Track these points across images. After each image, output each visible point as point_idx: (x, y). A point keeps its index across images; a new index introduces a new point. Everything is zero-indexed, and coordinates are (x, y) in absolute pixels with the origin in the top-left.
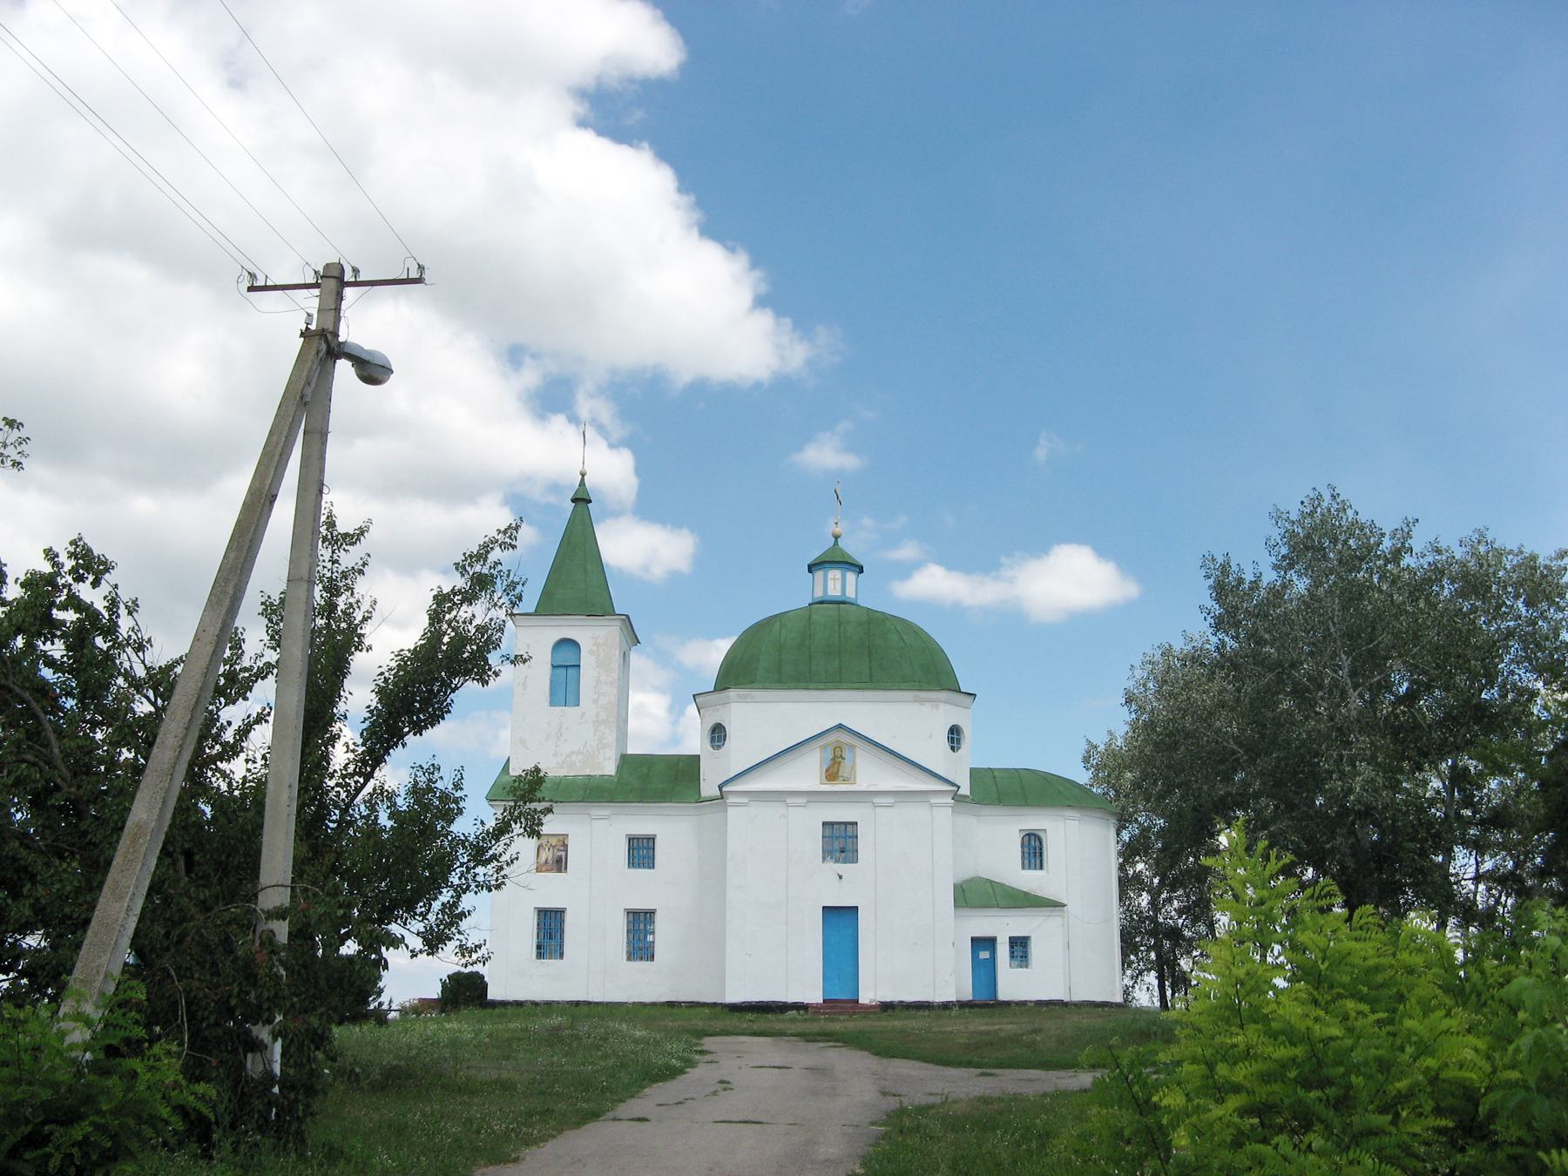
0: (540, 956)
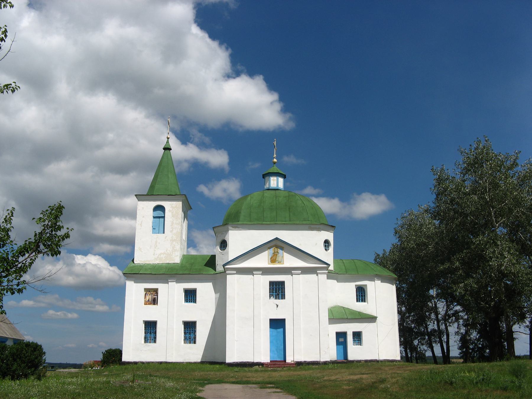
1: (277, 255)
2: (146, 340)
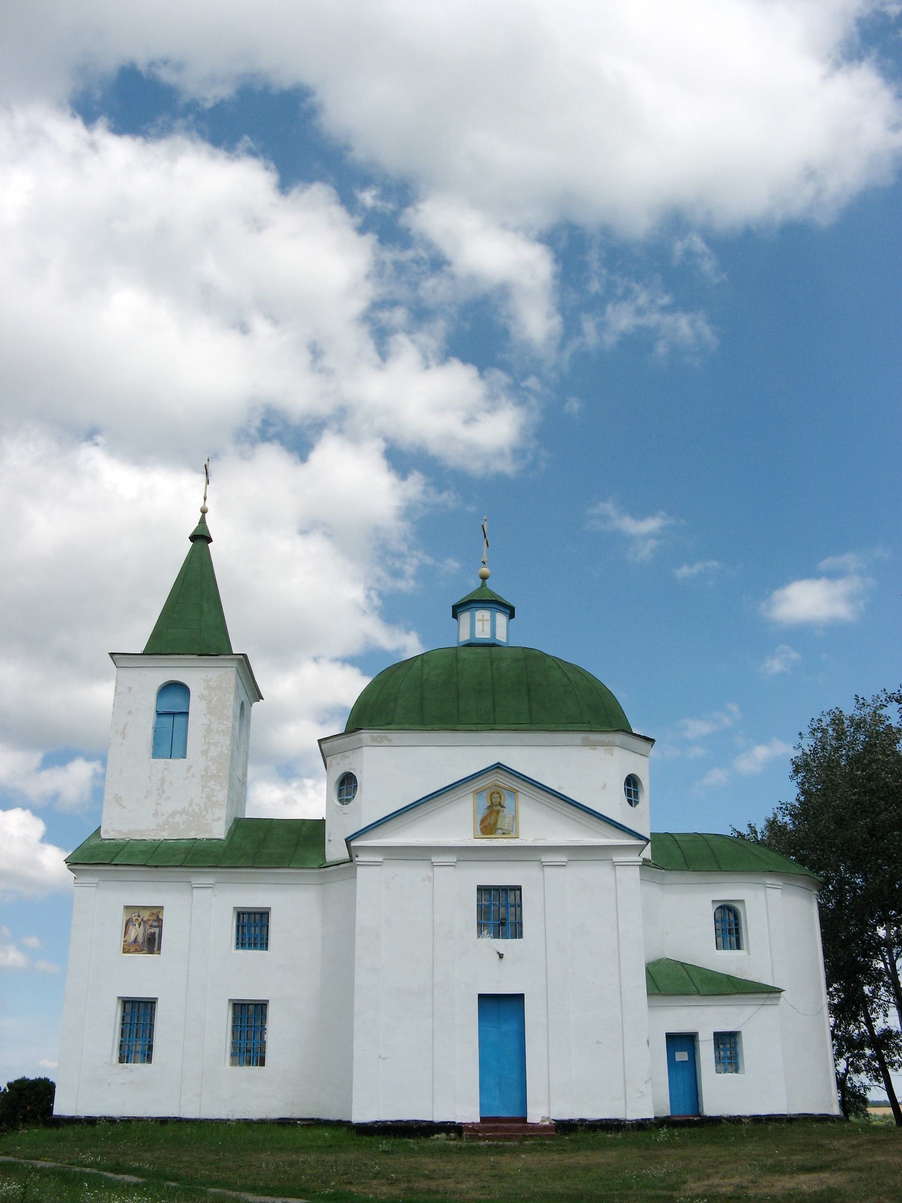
1: (498, 812)
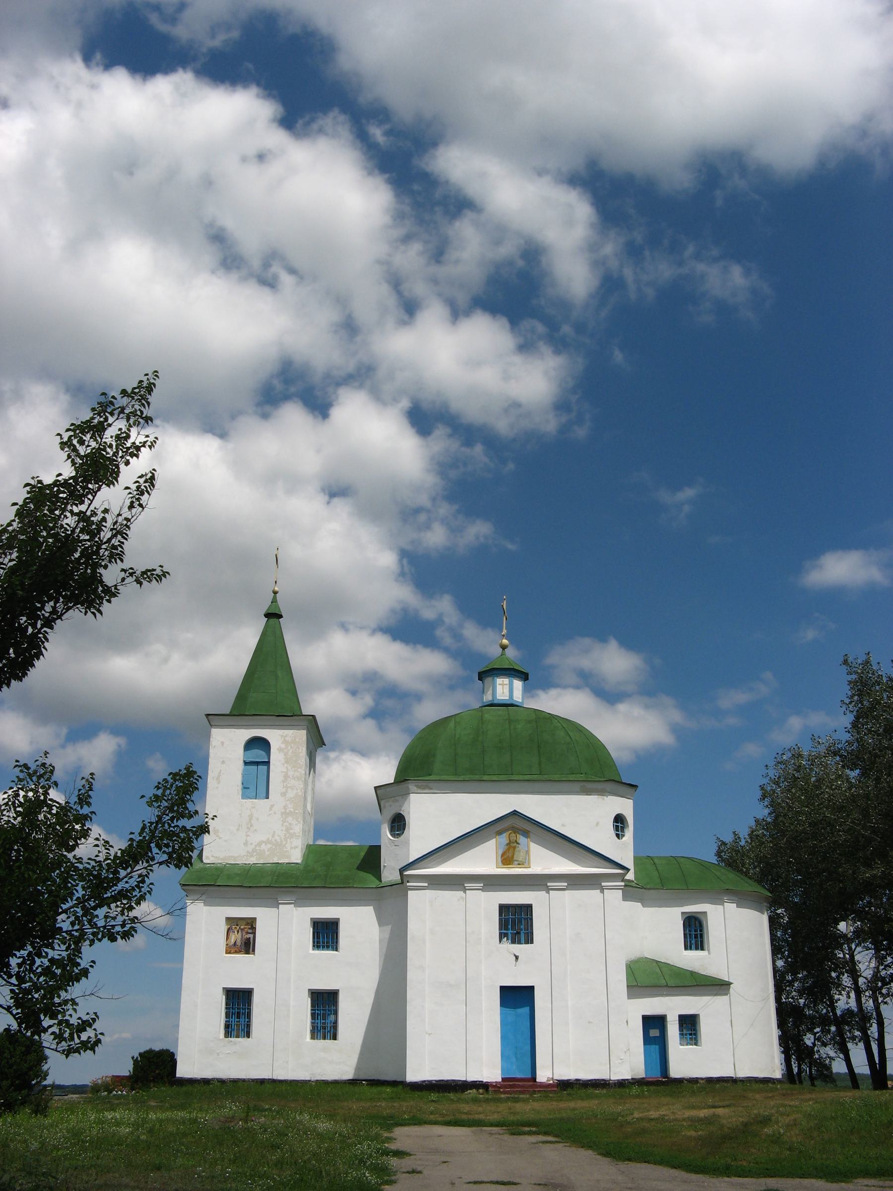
0: (228, 1034)
1: (515, 847)
2: (229, 1031)
